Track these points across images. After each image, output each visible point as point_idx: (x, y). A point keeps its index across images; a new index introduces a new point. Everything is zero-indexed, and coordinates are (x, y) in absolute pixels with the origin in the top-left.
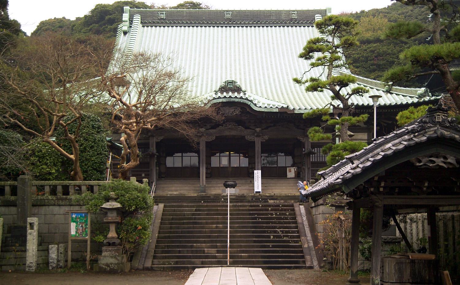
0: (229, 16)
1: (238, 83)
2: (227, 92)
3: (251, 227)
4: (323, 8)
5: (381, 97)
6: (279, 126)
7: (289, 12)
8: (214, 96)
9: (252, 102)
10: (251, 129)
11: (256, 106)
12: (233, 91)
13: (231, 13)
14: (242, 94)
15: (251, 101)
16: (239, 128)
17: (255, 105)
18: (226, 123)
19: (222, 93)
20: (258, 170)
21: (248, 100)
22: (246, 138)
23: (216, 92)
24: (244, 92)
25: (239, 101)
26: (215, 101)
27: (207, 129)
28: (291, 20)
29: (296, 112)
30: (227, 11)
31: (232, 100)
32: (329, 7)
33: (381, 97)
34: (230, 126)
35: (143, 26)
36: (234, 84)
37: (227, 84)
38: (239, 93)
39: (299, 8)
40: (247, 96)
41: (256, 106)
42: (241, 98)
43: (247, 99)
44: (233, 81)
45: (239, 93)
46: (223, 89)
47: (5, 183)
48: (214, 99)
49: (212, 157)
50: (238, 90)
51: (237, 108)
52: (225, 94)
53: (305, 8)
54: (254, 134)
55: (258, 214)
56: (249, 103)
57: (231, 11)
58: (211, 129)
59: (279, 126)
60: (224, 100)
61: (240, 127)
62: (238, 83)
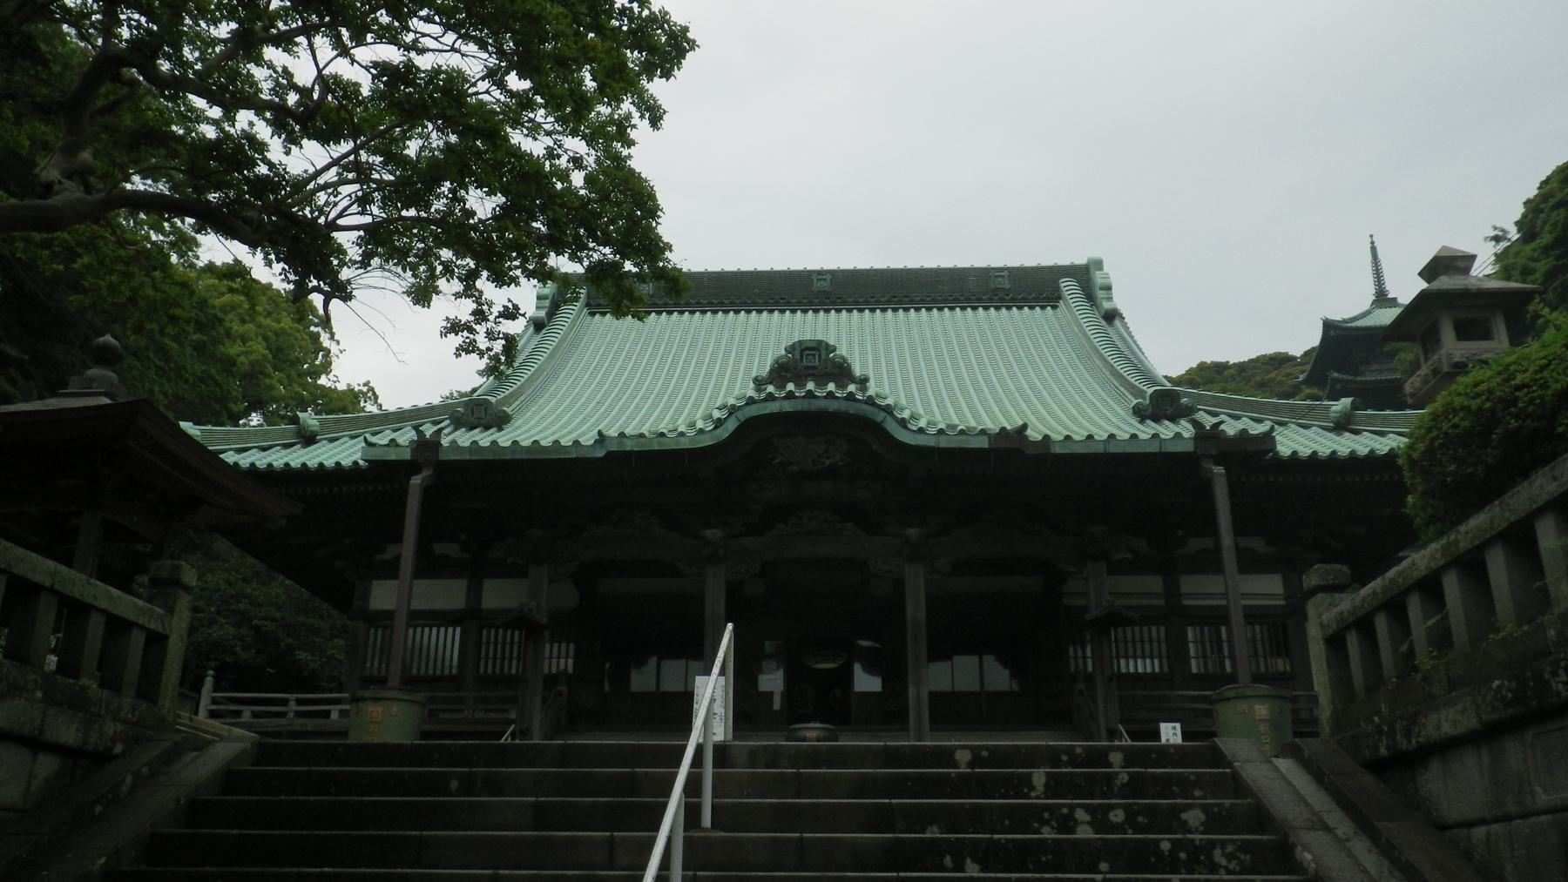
0: (825, 285)
1: (843, 351)
2: (800, 382)
3: (862, 787)
4: (1081, 260)
7: (986, 274)
8: (751, 393)
9: (891, 414)
11: (905, 427)
12: (821, 381)
13: (828, 277)
14: (852, 388)
15: (888, 410)
17: (903, 423)
19: (781, 387)
21: (874, 404)
23: (759, 383)
24: (863, 382)
26: (753, 411)
28: (995, 291)
29: (1057, 450)
32: (1095, 255)
35: (593, 314)
36: (823, 353)
37: (797, 353)
38: (841, 386)
39: (1014, 261)
40: (871, 392)
41: (905, 427)
42: (851, 397)
43: (870, 401)
44: (820, 342)
45: (841, 386)
46: (782, 372)
48: (751, 401)
50: (842, 372)
53: (1030, 262)
55: (953, 820)
56: (880, 416)
60: (788, 406)
61: (849, 525)
62: (844, 353)
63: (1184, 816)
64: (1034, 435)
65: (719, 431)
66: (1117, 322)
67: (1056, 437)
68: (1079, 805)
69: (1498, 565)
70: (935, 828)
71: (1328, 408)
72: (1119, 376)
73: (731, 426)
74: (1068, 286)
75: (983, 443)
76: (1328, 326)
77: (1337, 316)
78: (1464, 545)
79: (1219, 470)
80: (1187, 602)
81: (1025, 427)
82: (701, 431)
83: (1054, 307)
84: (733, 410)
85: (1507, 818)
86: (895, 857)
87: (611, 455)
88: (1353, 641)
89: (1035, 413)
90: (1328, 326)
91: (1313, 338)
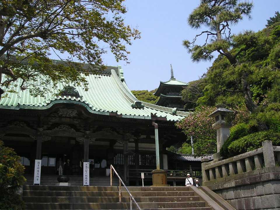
2: (67, 95)
5: (156, 113)
6: (105, 130)
9: (88, 105)
10: (81, 132)
12: (72, 96)
14: (79, 99)
15: (88, 105)
16: (72, 130)
17: (91, 108)
18: (61, 126)
20: (38, 159)
22: (77, 139)
25: (78, 103)
27: (44, 130)
29: (123, 117)
30: (54, 60)
31: (71, 102)
33: (156, 113)
34: (64, 128)
36: (73, 90)
38: (77, 98)
45: (77, 98)
46: (62, 93)
47: (221, 110)
49: (107, 169)
50: (77, 95)
51: (73, 110)
52: (65, 97)
54: (83, 136)
57: (56, 60)
58: (47, 129)
59: (105, 130)
61: (72, 129)
63: (190, 199)
64: (119, 113)
65: (48, 106)
66: (124, 82)
67: (124, 114)
68: (175, 197)
69: (239, 165)
70: (154, 201)
71: (171, 110)
72: (127, 96)
73: (51, 105)
74: (113, 71)
75: (108, 114)
76: (161, 83)
77: (163, 81)
78: (234, 160)
79: (156, 124)
80: (140, 149)
81: (117, 111)
82: (43, 106)
83: (110, 76)
84: (51, 101)
85: (237, 199)
86: (184, 205)
87: (21, 109)
88: (211, 172)
89: (118, 109)
90: (161, 83)
91: (157, 86)
